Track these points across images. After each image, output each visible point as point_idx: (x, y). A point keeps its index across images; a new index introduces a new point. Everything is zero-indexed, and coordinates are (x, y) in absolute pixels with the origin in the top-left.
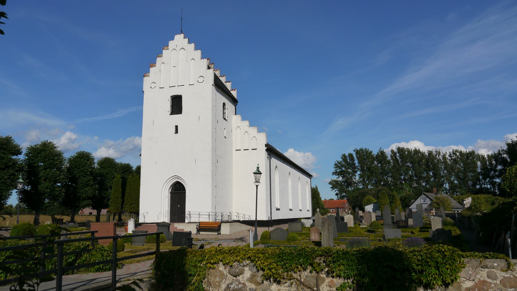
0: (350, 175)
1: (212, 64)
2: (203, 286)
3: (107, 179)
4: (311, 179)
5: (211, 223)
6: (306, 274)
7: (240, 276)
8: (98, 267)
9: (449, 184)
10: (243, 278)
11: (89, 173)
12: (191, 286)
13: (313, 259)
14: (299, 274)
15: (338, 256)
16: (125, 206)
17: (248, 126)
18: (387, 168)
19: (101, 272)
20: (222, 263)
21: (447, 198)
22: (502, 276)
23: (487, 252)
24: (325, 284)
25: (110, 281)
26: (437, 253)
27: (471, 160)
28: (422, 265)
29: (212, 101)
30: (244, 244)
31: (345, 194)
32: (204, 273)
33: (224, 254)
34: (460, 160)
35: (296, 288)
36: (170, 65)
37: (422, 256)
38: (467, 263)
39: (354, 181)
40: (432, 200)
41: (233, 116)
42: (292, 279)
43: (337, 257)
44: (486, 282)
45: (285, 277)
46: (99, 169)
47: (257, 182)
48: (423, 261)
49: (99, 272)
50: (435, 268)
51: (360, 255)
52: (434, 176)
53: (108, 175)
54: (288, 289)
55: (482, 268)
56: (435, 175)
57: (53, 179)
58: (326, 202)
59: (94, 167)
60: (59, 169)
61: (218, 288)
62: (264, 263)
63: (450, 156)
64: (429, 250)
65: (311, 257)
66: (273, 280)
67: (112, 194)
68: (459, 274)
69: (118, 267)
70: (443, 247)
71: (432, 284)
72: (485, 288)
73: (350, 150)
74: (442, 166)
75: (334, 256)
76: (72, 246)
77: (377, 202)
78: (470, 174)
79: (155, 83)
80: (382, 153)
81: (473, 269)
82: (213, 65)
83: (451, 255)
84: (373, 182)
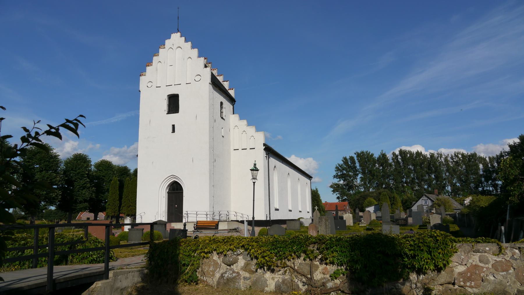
0: (351, 178)
1: (209, 63)
2: (197, 275)
3: (104, 182)
4: (310, 180)
5: (209, 222)
6: (299, 262)
7: (234, 265)
8: (92, 259)
9: (451, 186)
10: (237, 267)
11: (86, 176)
12: (185, 276)
13: (307, 247)
14: (293, 262)
15: (332, 242)
16: (123, 209)
17: (246, 126)
18: (389, 171)
19: (95, 263)
20: (216, 252)
21: (448, 199)
22: (494, 260)
23: (479, 237)
24: (319, 271)
25: (103, 269)
26: (430, 238)
27: (473, 162)
28: (414, 250)
29: (209, 100)
30: (238, 234)
31: (346, 198)
32: (198, 262)
33: (218, 243)
34: (462, 163)
35: (290, 276)
36: (167, 64)
37: (414, 241)
38: (459, 248)
39: (355, 185)
40: (434, 201)
41: (231, 115)
42: (286, 267)
43: (330, 243)
44: (479, 266)
45: (279, 265)
46: (96, 172)
47: (254, 179)
48: (416, 246)
49: (93, 263)
50: (428, 253)
51: (353, 242)
52: (437, 178)
53: (105, 178)
54: (282, 277)
55: (474, 252)
56: (437, 178)
57: (49, 181)
58: (327, 204)
59: (91, 170)
60: (56, 171)
61: (212, 277)
62: (257, 251)
63: (451, 158)
64: (421, 235)
65: (305, 245)
66: (267, 268)
67: (109, 197)
68: (451, 259)
69: (112, 260)
70: (436, 232)
71: (424, 268)
72: (477, 272)
73: (351, 153)
74: (444, 169)
75: (328, 243)
76: (66, 238)
77: (378, 204)
78: (472, 177)
79: (152, 82)
80: (384, 156)
81: (465, 253)
82: (210, 64)
83: (443, 240)
84: (375, 185)
